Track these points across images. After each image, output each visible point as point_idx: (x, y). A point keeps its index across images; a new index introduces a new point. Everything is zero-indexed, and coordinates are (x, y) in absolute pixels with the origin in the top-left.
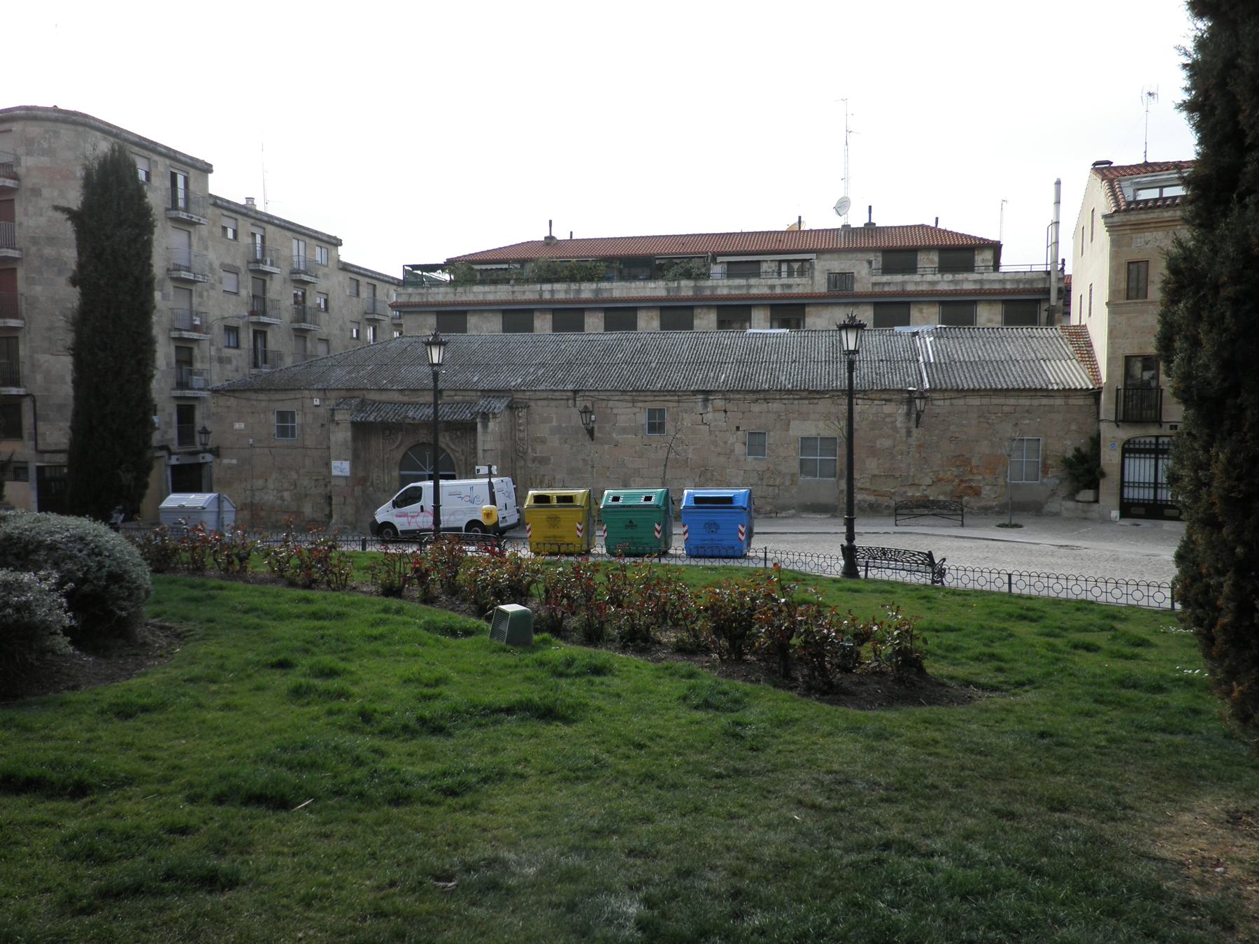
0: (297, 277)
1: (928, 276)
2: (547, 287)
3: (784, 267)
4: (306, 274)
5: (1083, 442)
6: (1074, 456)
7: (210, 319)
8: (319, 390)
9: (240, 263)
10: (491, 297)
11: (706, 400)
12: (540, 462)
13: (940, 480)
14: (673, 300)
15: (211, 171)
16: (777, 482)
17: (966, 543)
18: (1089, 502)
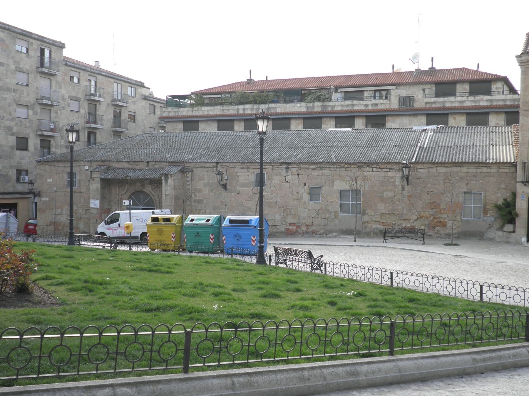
0: (115, 103)
1: (463, 98)
2: (241, 107)
3: (377, 94)
4: (120, 101)
5: (508, 195)
6: (503, 204)
7: (61, 125)
8: (88, 161)
9: (80, 95)
10: (211, 113)
11: (288, 168)
12: (198, 202)
13: (422, 217)
14: (310, 113)
15: (64, 47)
16: (327, 217)
17: (407, 252)
18: (511, 232)
